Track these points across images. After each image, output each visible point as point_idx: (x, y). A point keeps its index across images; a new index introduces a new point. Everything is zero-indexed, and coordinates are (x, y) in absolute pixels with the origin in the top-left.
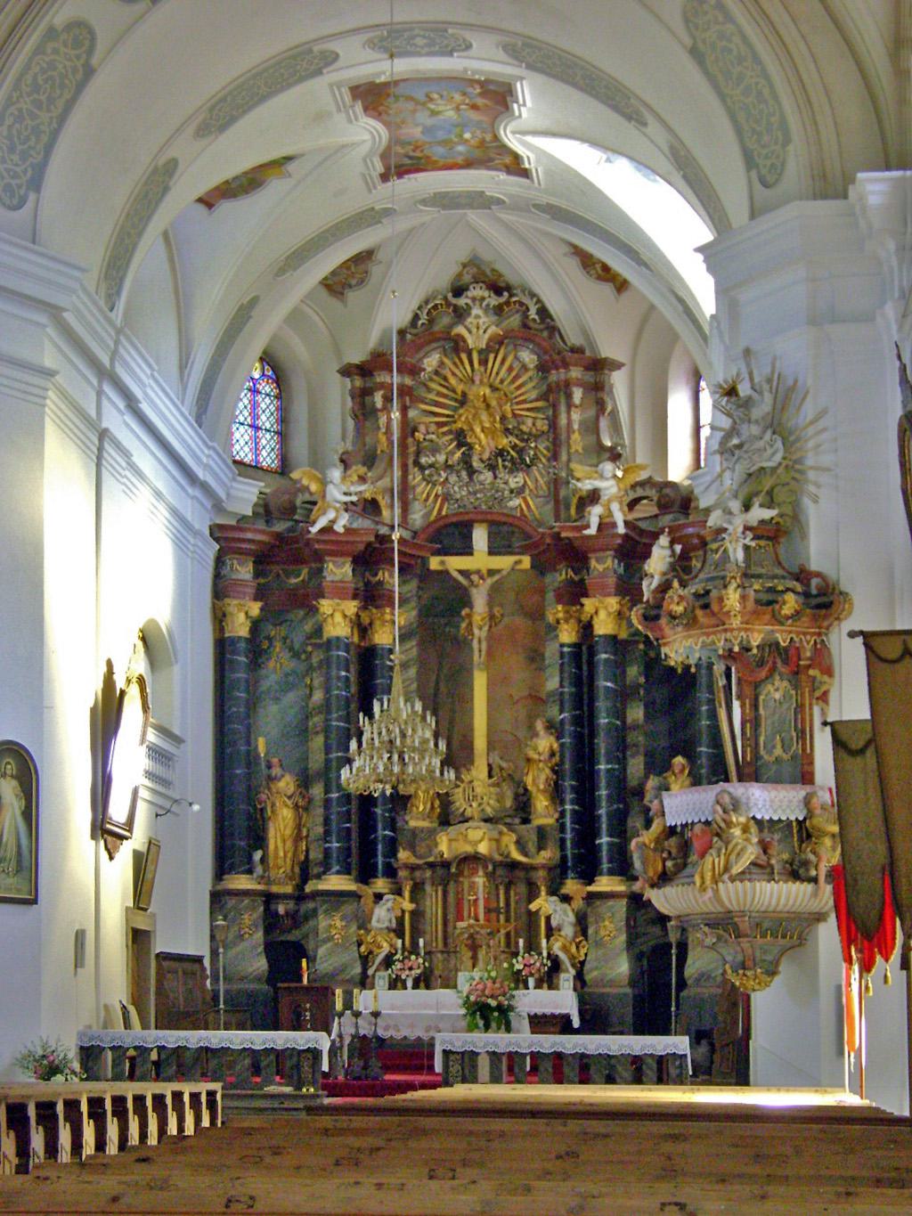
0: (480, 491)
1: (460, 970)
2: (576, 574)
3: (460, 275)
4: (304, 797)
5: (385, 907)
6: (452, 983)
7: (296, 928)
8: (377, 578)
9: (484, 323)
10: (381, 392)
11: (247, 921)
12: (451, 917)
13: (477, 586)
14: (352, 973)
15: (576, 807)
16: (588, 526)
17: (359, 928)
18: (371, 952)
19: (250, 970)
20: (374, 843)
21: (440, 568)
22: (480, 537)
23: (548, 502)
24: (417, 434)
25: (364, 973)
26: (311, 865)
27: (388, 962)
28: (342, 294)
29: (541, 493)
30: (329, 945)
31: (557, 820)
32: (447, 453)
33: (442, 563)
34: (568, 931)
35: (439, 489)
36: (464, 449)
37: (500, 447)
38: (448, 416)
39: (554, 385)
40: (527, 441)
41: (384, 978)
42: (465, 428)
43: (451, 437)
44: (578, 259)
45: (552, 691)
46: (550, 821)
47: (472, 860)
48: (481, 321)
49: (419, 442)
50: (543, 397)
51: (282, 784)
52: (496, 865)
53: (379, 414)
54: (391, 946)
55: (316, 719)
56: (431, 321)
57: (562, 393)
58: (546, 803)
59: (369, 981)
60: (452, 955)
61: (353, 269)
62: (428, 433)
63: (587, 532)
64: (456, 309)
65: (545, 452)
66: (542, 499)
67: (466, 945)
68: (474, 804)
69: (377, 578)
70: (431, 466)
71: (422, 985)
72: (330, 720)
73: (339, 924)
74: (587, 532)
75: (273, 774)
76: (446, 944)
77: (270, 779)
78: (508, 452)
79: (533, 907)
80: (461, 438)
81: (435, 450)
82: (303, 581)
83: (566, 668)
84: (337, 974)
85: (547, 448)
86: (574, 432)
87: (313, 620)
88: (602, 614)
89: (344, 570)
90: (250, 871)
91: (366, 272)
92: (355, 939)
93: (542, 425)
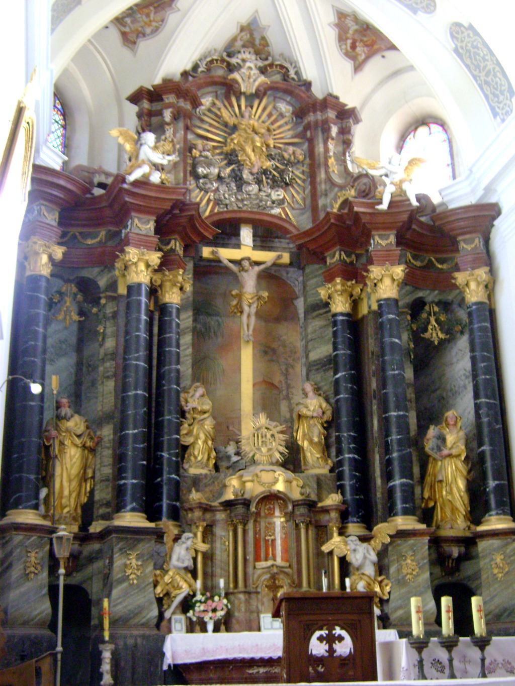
0: (247, 199)
1: (261, 612)
2: (347, 256)
3: (234, 40)
4: (91, 438)
5: (184, 546)
6: (255, 626)
7: (78, 571)
8: (169, 247)
9: (254, 74)
10: (170, 110)
11: (33, 559)
12: (250, 557)
13: (246, 271)
14: (148, 616)
15: (356, 456)
16: (381, 203)
17: (155, 569)
18: (167, 594)
19: (35, 613)
20: (160, 485)
21: (211, 257)
22: (246, 234)
23: (303, 214)
24: (194, 151)
25: (161, 616)
26: (96, 506)
27: (187, 605)
28: (135, 43)
29: (296, 206)
30: (125, 585)
31: (331, 471)
32: (219, 168)
33: (213, 253)
34: (370, 570)
35: (211, 195)
36: (233, 166)
37: (264, 168)
38: (219, 142)
39: (312, 124)
40: (286, 165)
41: (180, 622)
42: (237, 148)
43: (222, 157)
44: (337, 30)
45: (315, 361)
46: (325, 471)
47: (271, 498)
48: (252, 72)
49: (194, 158)
50: (302, 135)
51: (70, 424)
52: (296, 504)
53: (167, 127)
54: (190, 586)
55: (108, 364)
56: (209, 70)
57: (320, 129)
58: (318, 456)
59: (164, 623)
60: (253, 596)
61: (152, 15)
62: (204, 150)
63: (380, 207)
64: (229, 64)
65: (301, 176)
66: (298, 211)
67: (266, 586)
68: (264, 450)
69: (169, 247)
70: (205, 176)
71: (223, 627)
72: (129, 359)
73: (134, 562)
74: (380, 207)
75: (63, 414)
76: (246, 586)
77: (59, 418)
78: (271, 172)
79: (326, 548)
80: (231, 158)
81: (209, 164)
82: (101, 241)
83: (340, 334)
84: (131, 618)
85: (303, 173)
86: (330, 157)
87: (109, 275)
88: (387, 281)
89: (148, 226)
90: (36, 507)
91: (162, 21)
92: (151, 580)
93: (300, 153)
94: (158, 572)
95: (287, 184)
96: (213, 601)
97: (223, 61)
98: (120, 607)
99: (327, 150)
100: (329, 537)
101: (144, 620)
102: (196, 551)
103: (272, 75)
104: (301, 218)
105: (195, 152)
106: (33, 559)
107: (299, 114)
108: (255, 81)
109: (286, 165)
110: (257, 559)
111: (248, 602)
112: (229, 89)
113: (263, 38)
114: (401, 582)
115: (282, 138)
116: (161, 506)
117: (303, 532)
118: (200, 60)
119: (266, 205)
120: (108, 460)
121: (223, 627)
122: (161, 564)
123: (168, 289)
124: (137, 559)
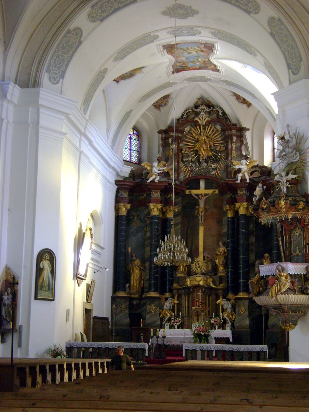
1: (193, 323)
4: (143, 267)
5: (169, 302)
11: (123, 306)
15: (232, 270)
21: (189, 193)
22: (202, 184)
27: (169, 320)
29: (222, 169)
32: (192, 157)
38: (192, 146)
42: (198, 149)
47: (198, 287)
51: (136, 262)
52: (205, 289)
57: (229, 138)
61: (163, 100)
62: (186, 151)
63: (237, 182)
65: (224, 157)
70: (187, 161)
71: (180, 328)
73: (153, 308)
74: (237, 182)
75: (133, 259)
78: (212, 157)
79: (218, 302)
81: (188, 156)
90: (125, 290)
93: (223, 148)
94: (161, 310)
95: (218, 161)
96: (176, 319)
97: (193, 111)
98: (149, 321)
99: (232, 147)
100: (219, 299)
101: (156, 325)
102: (175, 304)
103: (213, 115)
104: (223, 174)
105: (183, 152)
106: (123, 306)
107: (223, 131)
108: (205, 119)
109: (218, 153)
110: (193, 306)
111: (189, 320)
112: (196, 124)
113: (208, 100)
114: (239, 314)
115: (217, 141)
116: (166, 288)
117: (207, 298)
118: (184, 112)
119: (210, 170)
120: (148, 274)
121: (180, 328)
122: (162, 307)
123: (168, 212)
124: (154, 306)
